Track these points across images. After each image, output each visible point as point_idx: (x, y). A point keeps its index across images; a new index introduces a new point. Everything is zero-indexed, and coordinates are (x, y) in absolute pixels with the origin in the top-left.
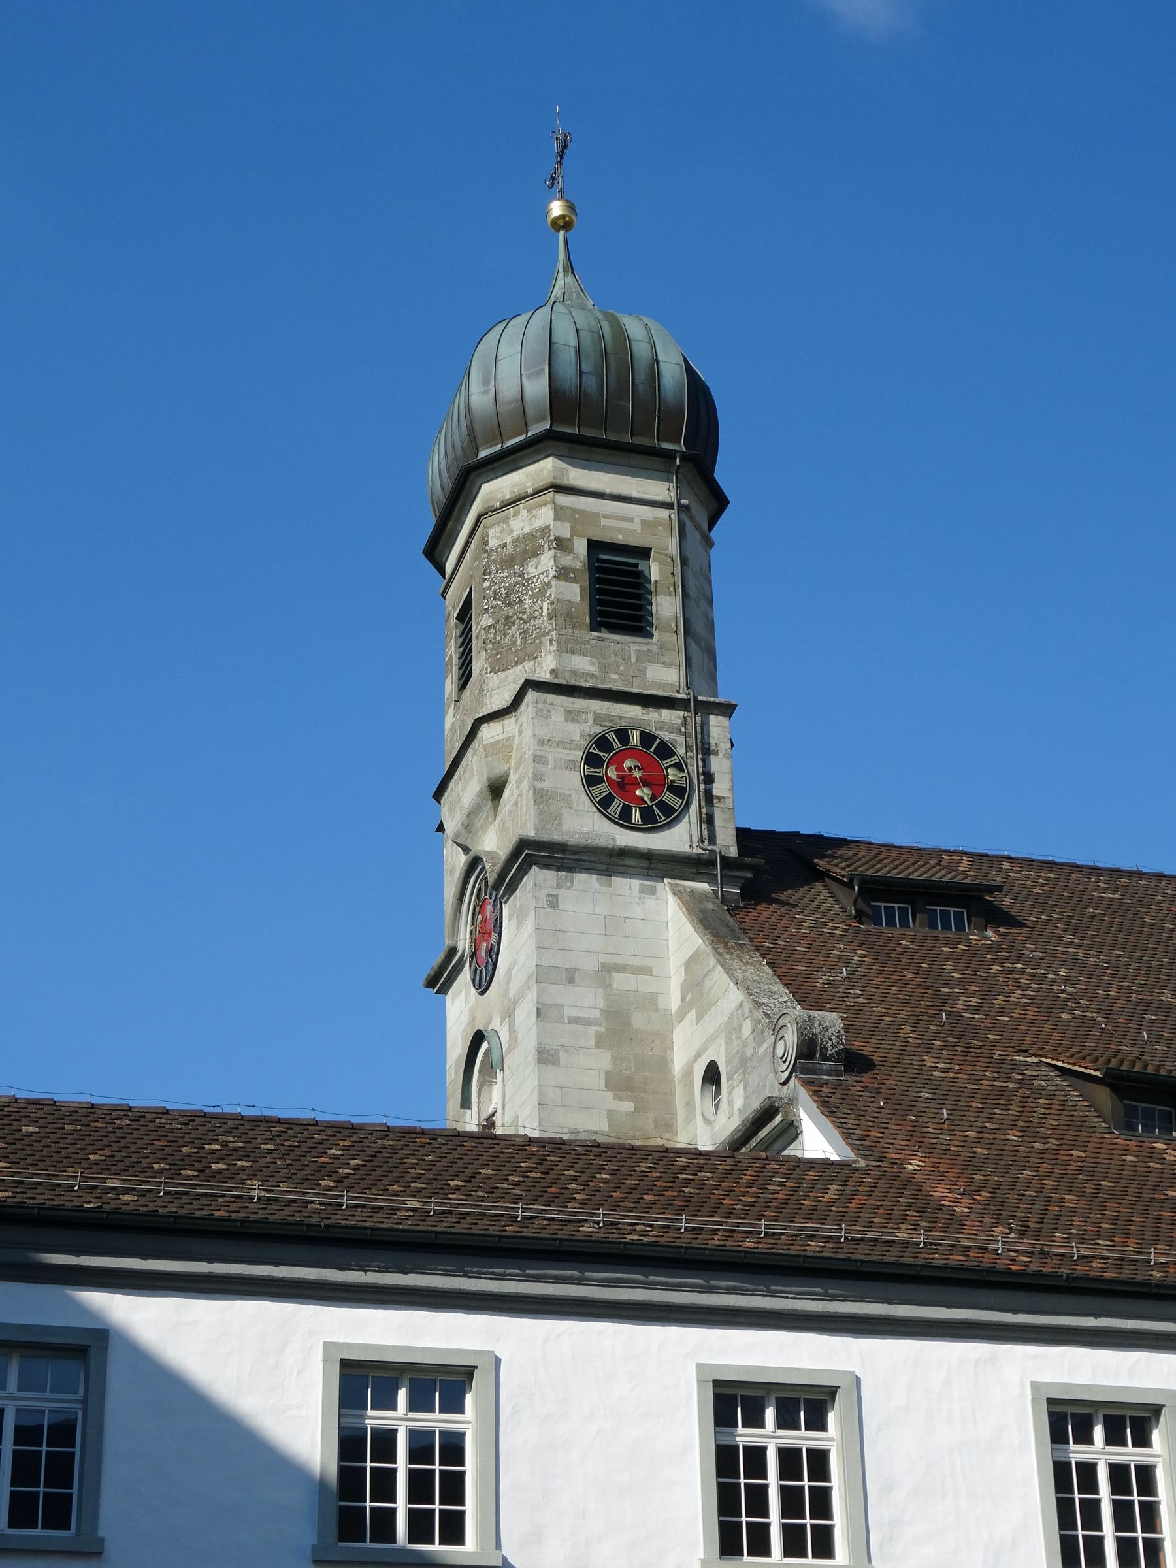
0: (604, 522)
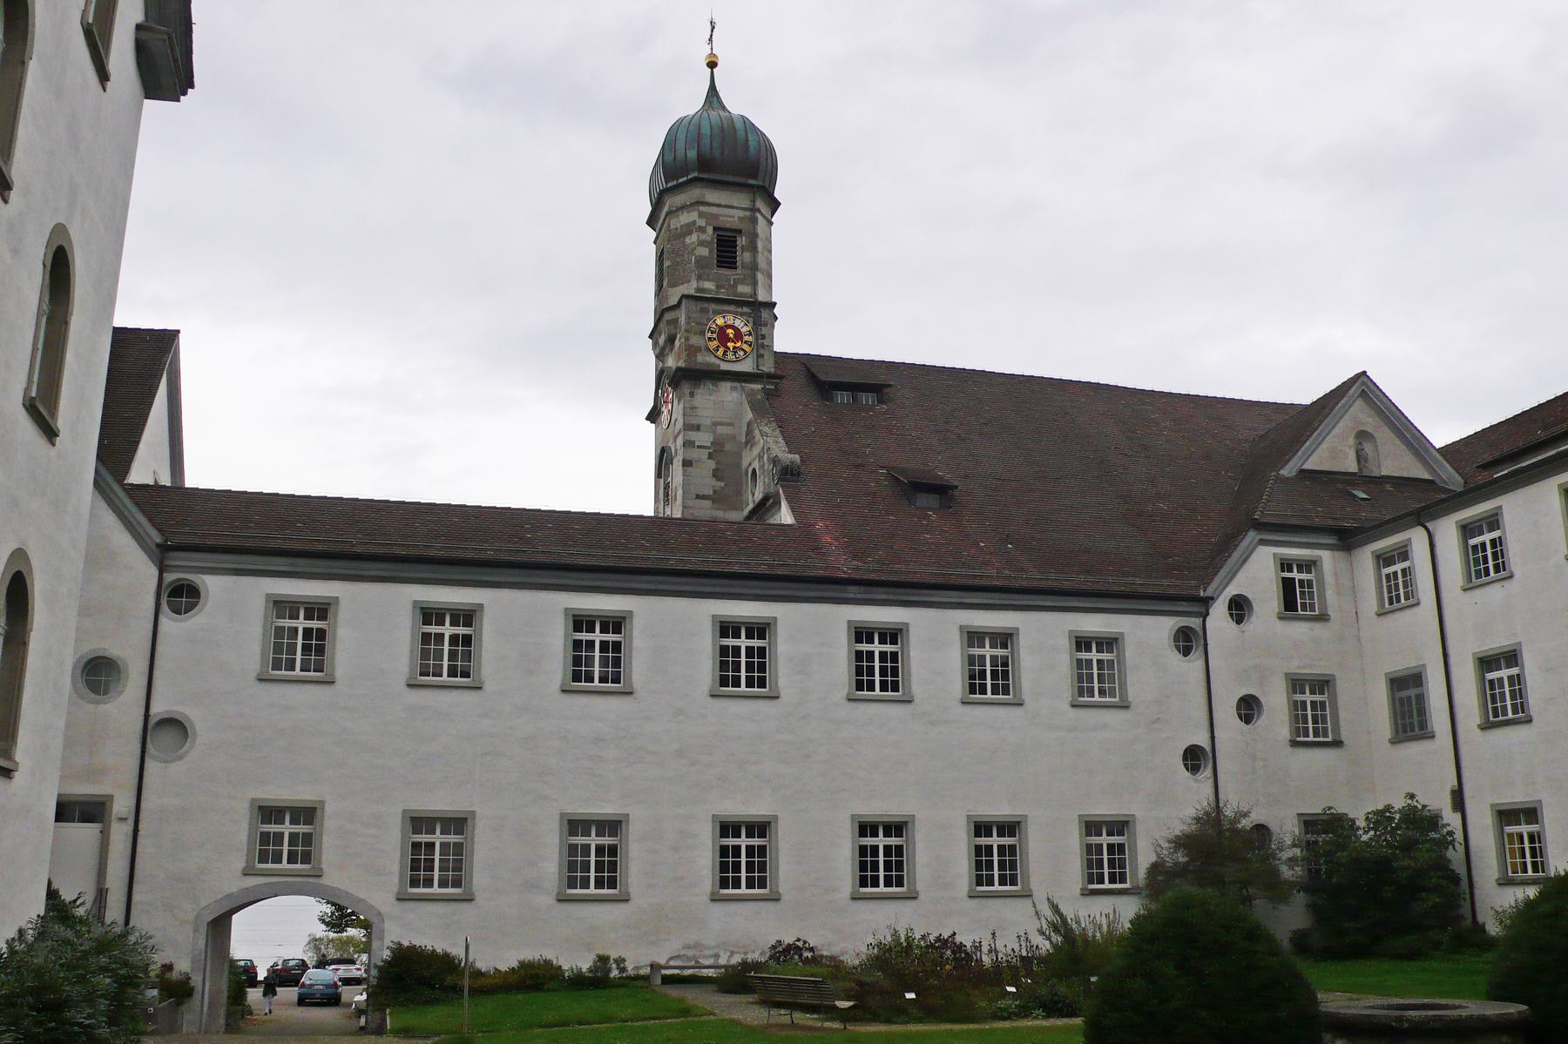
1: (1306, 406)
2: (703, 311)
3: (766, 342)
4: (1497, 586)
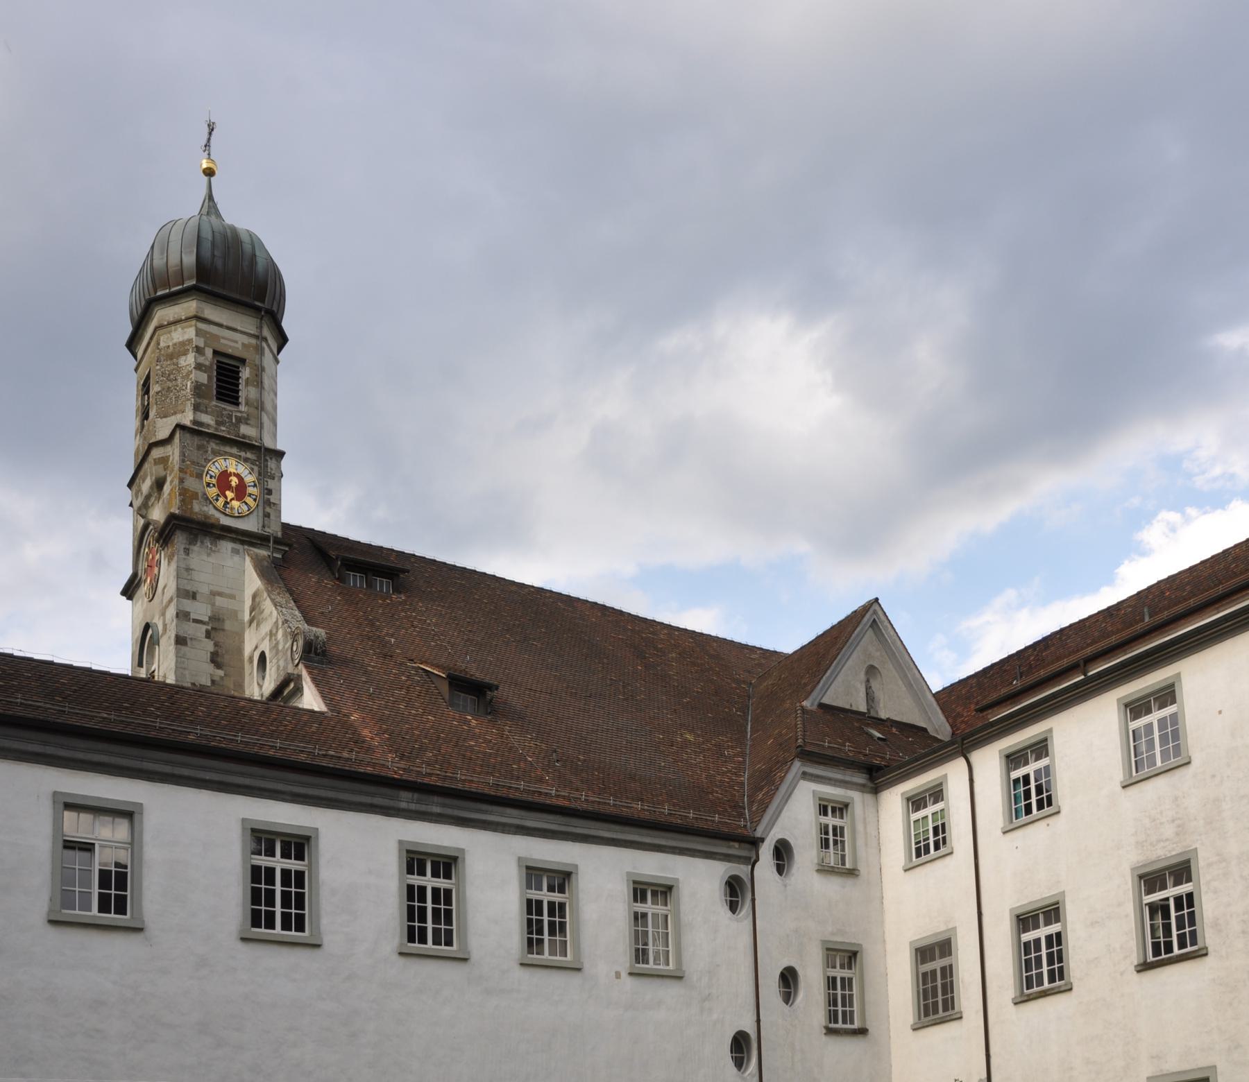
0: (222, 341)
1: (788, 657)
2: (199, 448)
3: (273, 499)
4: (1042, 824)
